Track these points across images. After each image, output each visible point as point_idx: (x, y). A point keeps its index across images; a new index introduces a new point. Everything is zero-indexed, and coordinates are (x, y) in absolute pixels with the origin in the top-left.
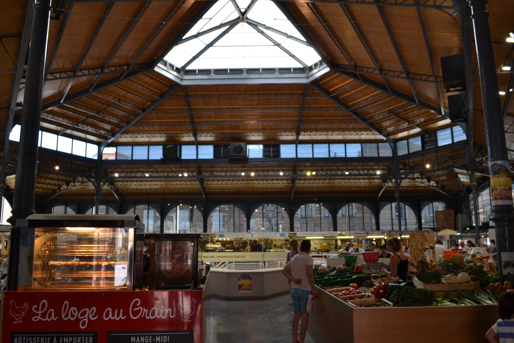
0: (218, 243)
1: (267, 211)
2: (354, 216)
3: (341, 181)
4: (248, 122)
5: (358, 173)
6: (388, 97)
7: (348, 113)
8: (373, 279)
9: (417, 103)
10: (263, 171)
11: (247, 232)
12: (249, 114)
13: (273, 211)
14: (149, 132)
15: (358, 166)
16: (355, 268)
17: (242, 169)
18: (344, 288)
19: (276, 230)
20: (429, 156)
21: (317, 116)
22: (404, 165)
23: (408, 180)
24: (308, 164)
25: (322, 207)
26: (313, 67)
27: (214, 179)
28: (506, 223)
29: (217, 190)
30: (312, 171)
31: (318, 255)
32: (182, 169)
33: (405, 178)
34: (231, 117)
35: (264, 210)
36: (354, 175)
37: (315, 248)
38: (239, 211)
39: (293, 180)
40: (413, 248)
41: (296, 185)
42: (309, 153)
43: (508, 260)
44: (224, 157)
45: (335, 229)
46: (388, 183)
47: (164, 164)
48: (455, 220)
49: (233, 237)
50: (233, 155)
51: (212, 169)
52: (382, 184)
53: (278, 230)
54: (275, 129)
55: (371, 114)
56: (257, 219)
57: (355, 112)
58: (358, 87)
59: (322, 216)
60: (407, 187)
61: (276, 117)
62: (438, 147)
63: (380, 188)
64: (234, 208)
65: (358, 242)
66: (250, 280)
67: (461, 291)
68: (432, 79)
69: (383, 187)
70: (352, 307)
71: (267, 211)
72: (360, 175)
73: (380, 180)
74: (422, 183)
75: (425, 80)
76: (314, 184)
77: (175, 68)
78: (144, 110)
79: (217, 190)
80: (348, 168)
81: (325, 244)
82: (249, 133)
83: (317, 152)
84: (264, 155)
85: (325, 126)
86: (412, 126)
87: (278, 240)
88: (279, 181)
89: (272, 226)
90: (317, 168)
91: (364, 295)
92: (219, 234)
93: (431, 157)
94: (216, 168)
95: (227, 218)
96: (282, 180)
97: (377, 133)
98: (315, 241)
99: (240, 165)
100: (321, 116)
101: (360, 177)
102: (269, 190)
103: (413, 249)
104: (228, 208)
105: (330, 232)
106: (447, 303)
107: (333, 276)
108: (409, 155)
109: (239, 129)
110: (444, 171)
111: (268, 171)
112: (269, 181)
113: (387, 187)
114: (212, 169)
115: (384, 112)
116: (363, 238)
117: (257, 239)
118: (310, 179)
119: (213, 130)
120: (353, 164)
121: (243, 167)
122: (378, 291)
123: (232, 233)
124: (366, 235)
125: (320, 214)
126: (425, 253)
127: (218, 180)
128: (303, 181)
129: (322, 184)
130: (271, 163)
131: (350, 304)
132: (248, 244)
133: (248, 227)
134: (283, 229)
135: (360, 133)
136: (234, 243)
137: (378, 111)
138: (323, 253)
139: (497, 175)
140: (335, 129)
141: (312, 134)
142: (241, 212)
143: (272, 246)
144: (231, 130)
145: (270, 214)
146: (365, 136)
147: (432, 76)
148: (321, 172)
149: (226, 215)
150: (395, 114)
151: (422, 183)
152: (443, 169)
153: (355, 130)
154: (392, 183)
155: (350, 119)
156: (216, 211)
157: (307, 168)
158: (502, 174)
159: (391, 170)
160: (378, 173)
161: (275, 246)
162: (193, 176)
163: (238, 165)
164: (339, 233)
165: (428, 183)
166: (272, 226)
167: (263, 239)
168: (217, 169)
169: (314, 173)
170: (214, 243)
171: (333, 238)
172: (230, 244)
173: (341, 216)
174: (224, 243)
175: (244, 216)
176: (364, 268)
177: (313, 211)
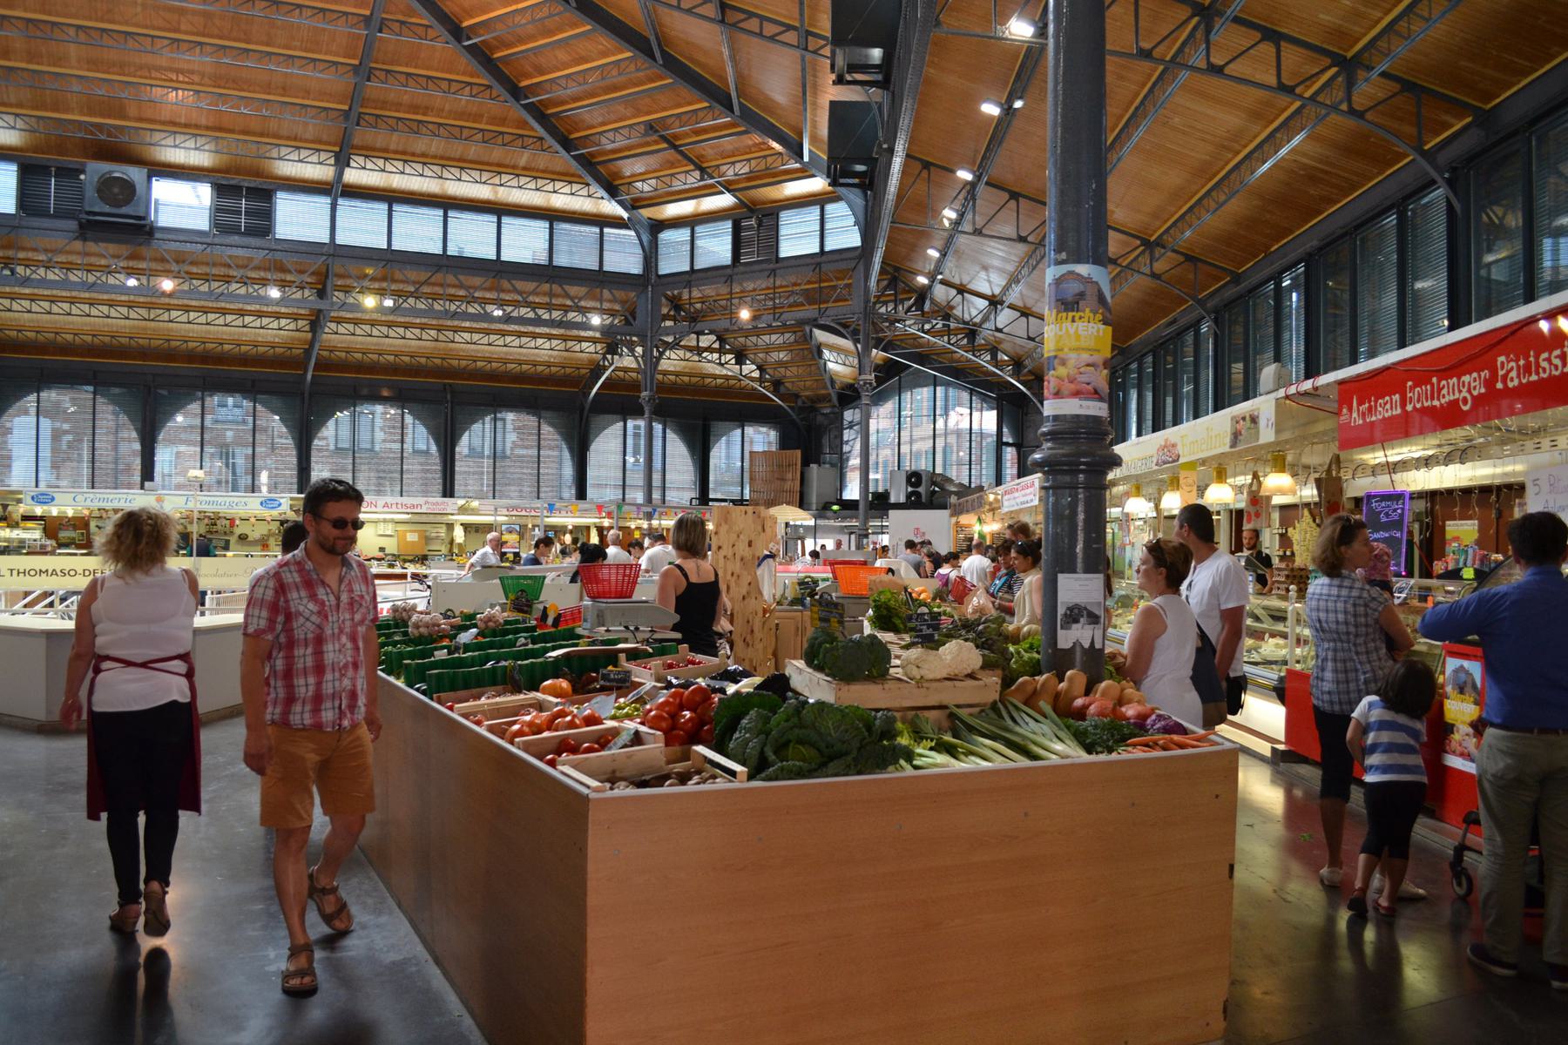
0: (30, 524)
1: (217, 421)
2: (508, 452)
3: (476, 337)
4: (157, 92)
5: (531, 315)
6: (652, 80)
7: (516, 111)
8: (628, 660)
9: (737, 112)
10: (206, 278)
11: (142, 487)
12: (163, 62)
13: (237, 423)
15: (534, 293)
16: (550, 621)
17: (131, 264)
18: (522, 696)
20: (750, 286)
21: (414, 108)
22: (676, 304)
23: (681, 353)
24: (369, 271)
25: (409, 419)
27: (17, 289)
28: (1081, 477)
30: (382, 293)
31: (390, 571)
33: (675, 345)
34: (94, 64)
35: (208, 418)
36: (522, 321)
37: (382, 549)
38: (116, 414)
39: (316, 322)
40: (722, 553)
43: (1078, 600)
44: (60, 214)
45: (448, 491)
46: (621, 355)
48: (803, 480)
49: (88, 503)
50: (96, 209)
51: (10, 253)
52: (605, 358)
53: (253, 488)
54: (262, 135)
55: (593, 127)
56: (182, 448)
57: (538, 112)
58: (560, 30)
59: (408, 446)
60: (677, 374)
61: (267, 88)
62: (778, 260)
63: (597, 370)
65: (519, 533)
67: (958, 706)
68: (791, 37)
69: (605, 369)
70: (585, 791)
71: (217, 421)
72: (538, 322)
73: (599, 347)
74: (721, 364)
75: (772, 38)
79: (31, 335)
80: (503, 296)
81: (412, 537)
82: (163, 135)
84: (216, 223)
85: (437, 146)
86: (712, 186)
87: (253, 520)
88: (265, 321)
89: (234, 473)
90: (401, 286)
91: (614, 728)
92: (34, 491)
93: (754, 290)
94: (23, 249)
95: (70, 437)
96: (278, 316)
97: (602, 193)
99: (124, 250)
100: (426, 110)
101: (538, 330)
103: (722, 561)
104: (74, 401)
105: (431, 500)
106: (935, 761)
107: (467, 648)
108: (693, 276)
109: (124, 117)
110: (787, 335)
111: (227, 280)
112: (229, 318)
113: (617, 369)
114: (10, 253)
115: (630, 126)
116: (538, 521)
118: (373, 323)
119: (20, 105)
120: (519, 285)
121: (132, 257)
122: (674, 716)
124: (545, 513)
125: (402, 442)
126: (759, 572)
127: (33, 298)
128: (350, 327)
129: (413, 343)
130: (240, 252)
131: (568, 772)
133: (148, 473)
134: (273, 487)
135: (550, 187)
136: (93, 524)
137: (616, 121)
138: (407, 565)
139: (1071, 314)
140: (471, 162)
141: (389, 167)
142: (123, 418)
143: (233, 540)
144: (91, 113)
145: (229, 434)
146: (563, 199)
147: (795, 28)
148: (411, 301)
149: (66, 426)
150: (664, 139)
151: (718, 367)
152: (784, 329)
153: (535, 173)
154: (636, 358)
155: (522, 136)
156: (26, 413)
157: (366, 283)
158: (1087, 310)
159: (634, 319)
160: (596, 320)
161: (243, 538)
163: (112, 248)
164: (461, 502)
166: (234, 473)
167: (196, 515)
168: (30, 255)
169: (389, 303)
170: (14, 525)
171: (439, 519)
172: (75, 528)
173: (466, 451)
174: (51, 527)
175: (134, 435)
176: (585, 621)
177: (377, 429)
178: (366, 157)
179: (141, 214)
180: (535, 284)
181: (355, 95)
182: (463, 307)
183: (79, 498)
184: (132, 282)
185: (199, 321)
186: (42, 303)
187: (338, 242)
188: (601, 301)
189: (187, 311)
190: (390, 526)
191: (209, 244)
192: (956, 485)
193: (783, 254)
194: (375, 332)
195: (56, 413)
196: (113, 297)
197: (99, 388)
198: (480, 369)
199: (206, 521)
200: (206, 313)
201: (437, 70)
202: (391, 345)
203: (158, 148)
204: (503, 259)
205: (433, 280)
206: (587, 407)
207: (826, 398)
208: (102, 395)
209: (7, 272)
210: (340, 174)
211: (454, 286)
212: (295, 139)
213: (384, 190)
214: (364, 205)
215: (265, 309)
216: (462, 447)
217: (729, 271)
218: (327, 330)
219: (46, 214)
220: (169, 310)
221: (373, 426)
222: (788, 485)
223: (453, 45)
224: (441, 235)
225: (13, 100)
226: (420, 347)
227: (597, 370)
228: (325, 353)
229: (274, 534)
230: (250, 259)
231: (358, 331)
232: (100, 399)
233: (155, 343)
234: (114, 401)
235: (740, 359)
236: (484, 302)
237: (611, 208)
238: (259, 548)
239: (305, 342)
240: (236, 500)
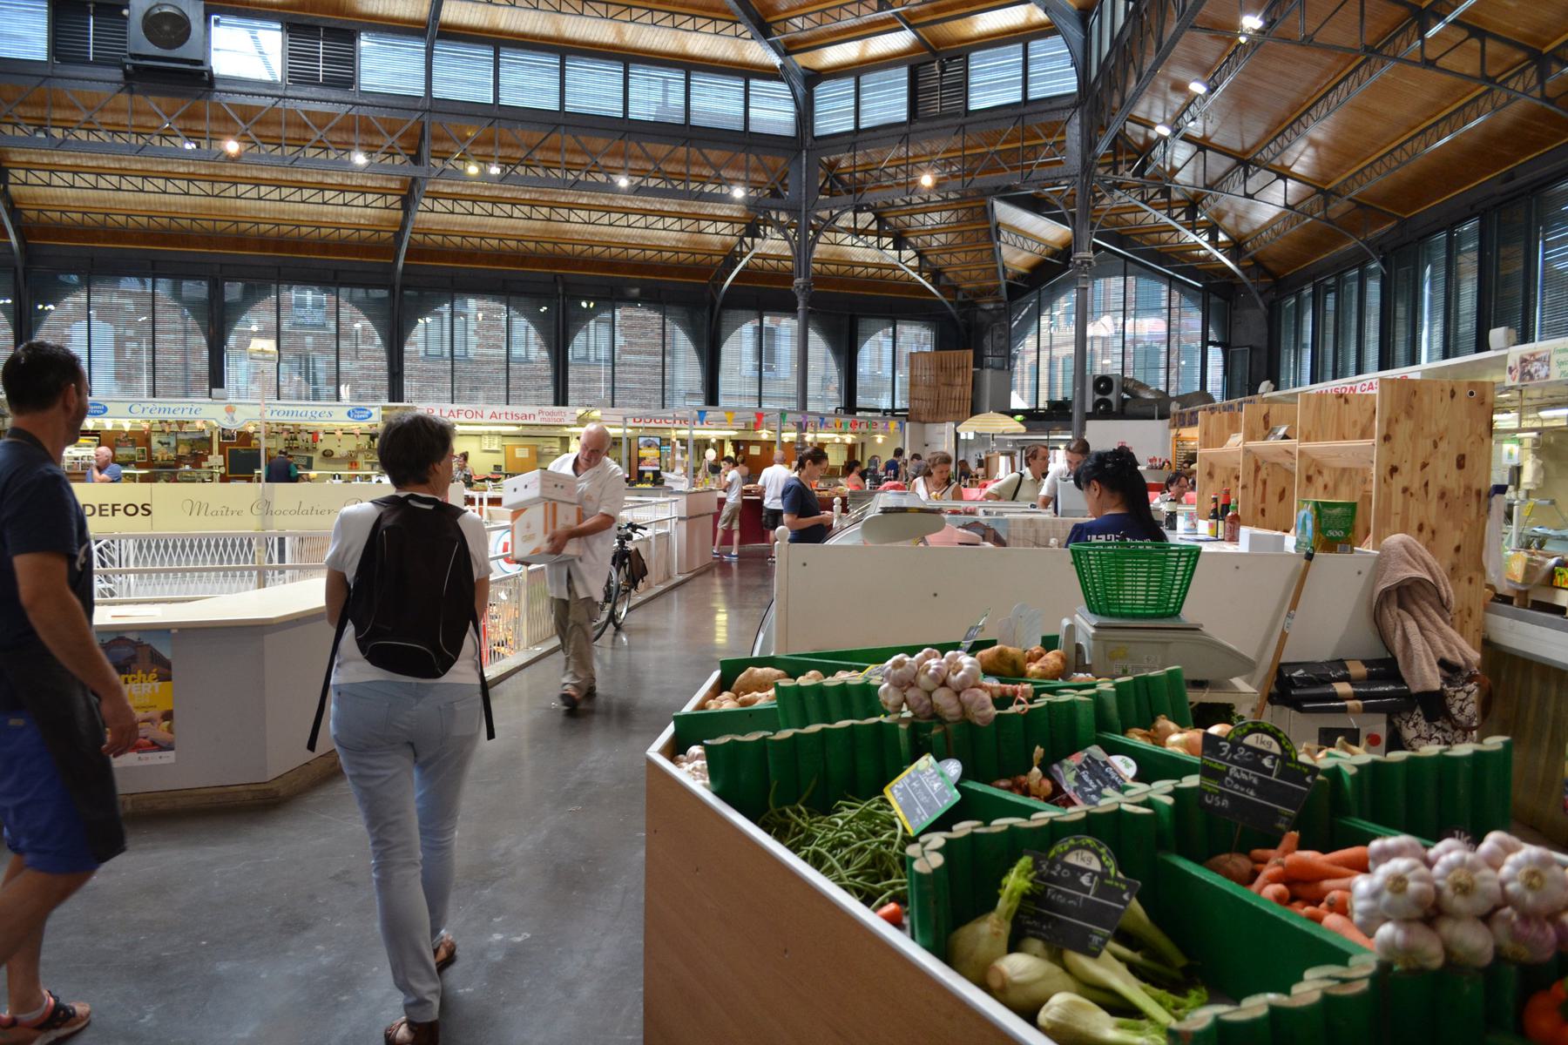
3: (595, 216)
11: (210, 396)
15: (668, 159)
17: (189, 125)
29: (74, 216)
30: (484, 160)
40: (1399, 481)
41: (419, 216)
42: (481, 84)
52: (741, 241)
62: (968, 112)
66: (165, 677)
69: (743, 255)
76: (491, 220)
83: (513, 82)
87: (339, 433)
88: (349, 196)
98: (486, 440)
99: (184, 105)
105: (546, 409)
108: (858, 137)
112: (307, 193)
113: (756, 256)
117: (251, 429)
123: (145, 398)
132: (216, 447)
133: (216, 378)
136: (154, 440)
143: (316, 457)
146: (702, 43)
161: (327, 455)
165: (896, 253)
171: (553, 432)
172: (134, 443)
179: (199, 58)
180: (668, 148)
183: (136, 408)
184: (189, 146)
185: (272, 196)
186: (86, 177)
187: (435, 95)
188: (747, 169)
189: (257, 185)
190: (497, 440)
191: (280, 97)
192: (1152, 392)
193: (972, 107)
194: (477, 210)
195: (108, 314)
199: (285, 435)
202: (495, 227)
204: (631, 116)
205: (546, 143)
206: (719, 301)
207: (992, 292)
209: (41, 135)
211: (573, 151)
213: (489, 31)
217: (904, 129)
218: (421, 207)
219: (84, 61)
220: (235, 184)
222: (957, 392)
224: (557, 87)
226: (528, 229)
227: (731, 257)
228: (419, 237)
229: (362, 451)
230: (331, 116)
231: (458, 209)
235: (899, 244)
236: (720, 181)
237: (759, 53)
238: (347, 466)
239: (395, 223)
240: (319, 410)
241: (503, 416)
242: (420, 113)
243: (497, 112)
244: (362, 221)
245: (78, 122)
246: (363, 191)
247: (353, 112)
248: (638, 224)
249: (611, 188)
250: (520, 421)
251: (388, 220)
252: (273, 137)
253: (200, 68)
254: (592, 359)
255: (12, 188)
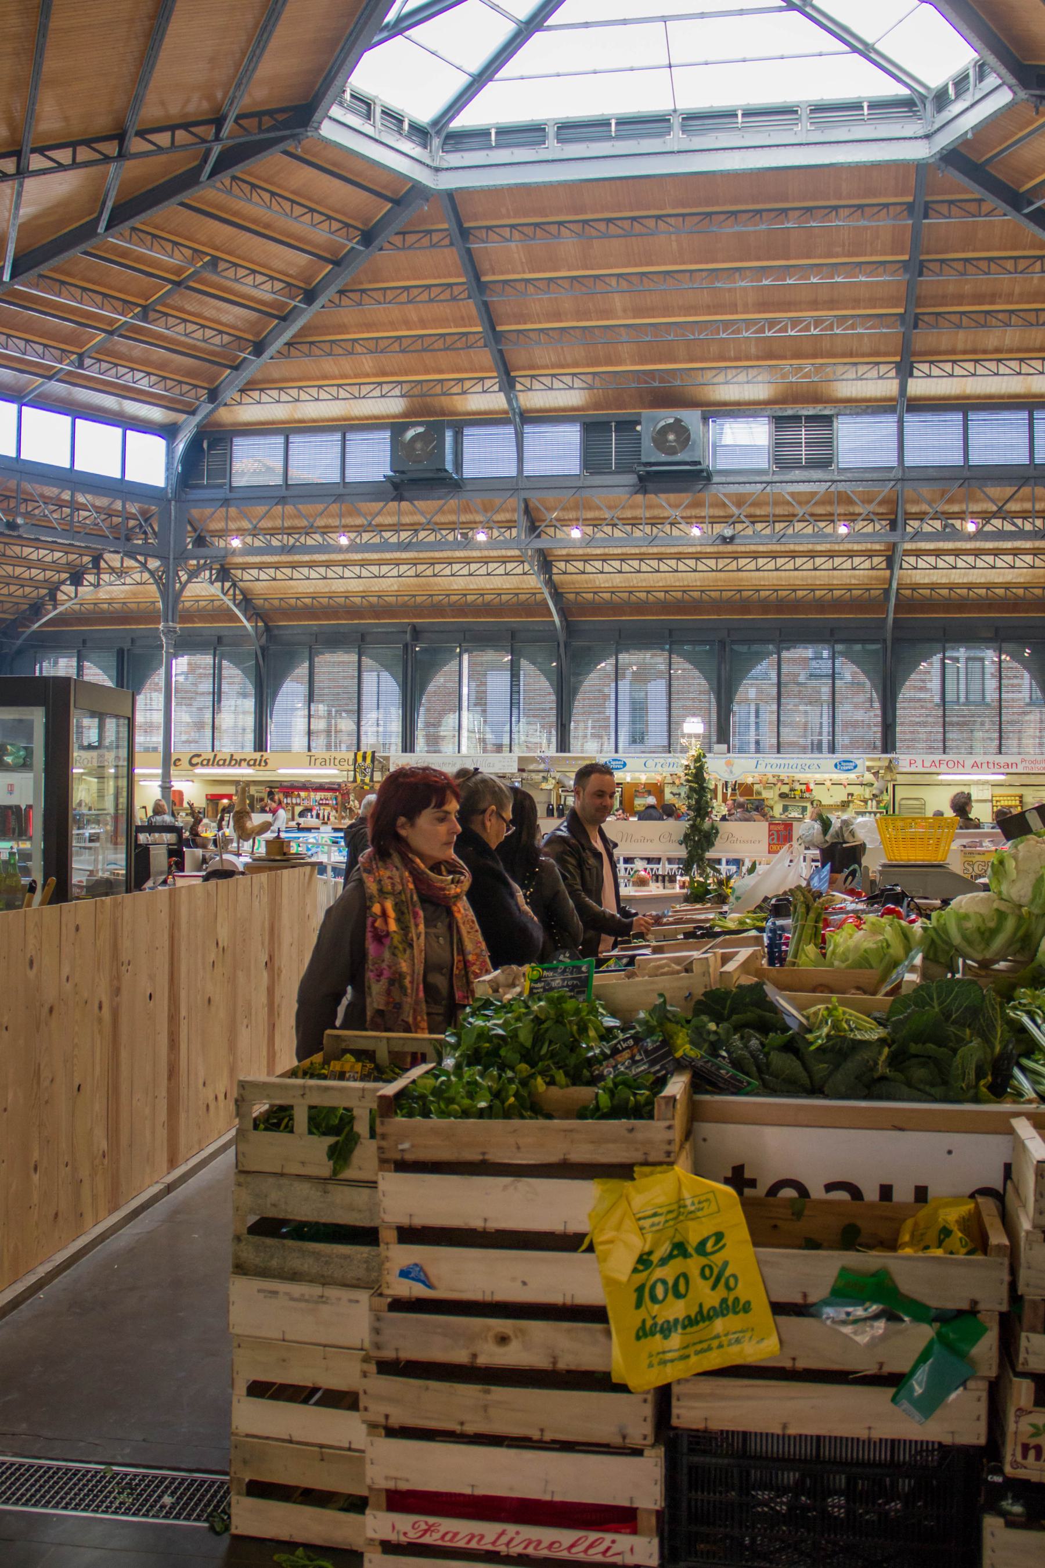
5: (377, 540)
14: (340, 381)
19: (771, 746)
21: (979, 298)
26: (951, 91)
32: (469, 517)
47: (400, 498)
50: (652, 460)
64: (670, 658)
72: (385, 547)
77: (406, 126)
78: (310, 297)
79: (606, 596)
82: (714, 372)
85: (1011, 337)
87: (828, 783)
99: (686, 498)
100: (993, 298)
102: (800, 594)
119: (576, 365)
136: (667, 790)
162: (506, 544)
165: (73, 588)
178: (931, 362)
181: (913, 297)
182: (302, 540)
183: (650, 763)
191: (768, 483)
196: (680, 549)
197: (675, 647)
198: (782, 600)
200: (775, 558)
201: (999, 249)
203: (706, 388)
208: (679, 655)
210: (903, 388)
212: (851, 355)
214: (936, 418)
215: (836, 547)
216: (906, 693)
220: (736, 558)
221: (983, 673)
223: (1012, 216)
225: (569, 360)
228: (908, 592)
230: (813, 494)
232: (675, 659)
233: (727, 595)
234: (689, 658)
236: (325, 530)
240: (809, 762)
241: (984, 766)
242: (893, 483)
243: (1032, 472)
244: (853, 582)
245: (605, 519)
246: (850, 555)
247: (832, 489)
248: (786, 567)
249: (958, 535)
250: (1002, 770)
251: (877, 578)
252: (825, 515)
253: (698, 467)
254: (962, 699)
255: (554, 577)
